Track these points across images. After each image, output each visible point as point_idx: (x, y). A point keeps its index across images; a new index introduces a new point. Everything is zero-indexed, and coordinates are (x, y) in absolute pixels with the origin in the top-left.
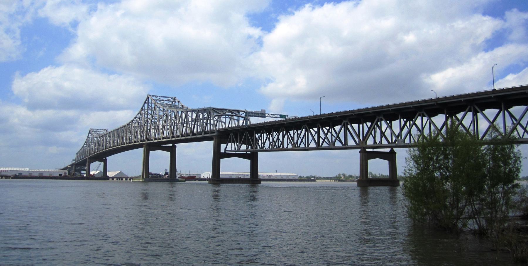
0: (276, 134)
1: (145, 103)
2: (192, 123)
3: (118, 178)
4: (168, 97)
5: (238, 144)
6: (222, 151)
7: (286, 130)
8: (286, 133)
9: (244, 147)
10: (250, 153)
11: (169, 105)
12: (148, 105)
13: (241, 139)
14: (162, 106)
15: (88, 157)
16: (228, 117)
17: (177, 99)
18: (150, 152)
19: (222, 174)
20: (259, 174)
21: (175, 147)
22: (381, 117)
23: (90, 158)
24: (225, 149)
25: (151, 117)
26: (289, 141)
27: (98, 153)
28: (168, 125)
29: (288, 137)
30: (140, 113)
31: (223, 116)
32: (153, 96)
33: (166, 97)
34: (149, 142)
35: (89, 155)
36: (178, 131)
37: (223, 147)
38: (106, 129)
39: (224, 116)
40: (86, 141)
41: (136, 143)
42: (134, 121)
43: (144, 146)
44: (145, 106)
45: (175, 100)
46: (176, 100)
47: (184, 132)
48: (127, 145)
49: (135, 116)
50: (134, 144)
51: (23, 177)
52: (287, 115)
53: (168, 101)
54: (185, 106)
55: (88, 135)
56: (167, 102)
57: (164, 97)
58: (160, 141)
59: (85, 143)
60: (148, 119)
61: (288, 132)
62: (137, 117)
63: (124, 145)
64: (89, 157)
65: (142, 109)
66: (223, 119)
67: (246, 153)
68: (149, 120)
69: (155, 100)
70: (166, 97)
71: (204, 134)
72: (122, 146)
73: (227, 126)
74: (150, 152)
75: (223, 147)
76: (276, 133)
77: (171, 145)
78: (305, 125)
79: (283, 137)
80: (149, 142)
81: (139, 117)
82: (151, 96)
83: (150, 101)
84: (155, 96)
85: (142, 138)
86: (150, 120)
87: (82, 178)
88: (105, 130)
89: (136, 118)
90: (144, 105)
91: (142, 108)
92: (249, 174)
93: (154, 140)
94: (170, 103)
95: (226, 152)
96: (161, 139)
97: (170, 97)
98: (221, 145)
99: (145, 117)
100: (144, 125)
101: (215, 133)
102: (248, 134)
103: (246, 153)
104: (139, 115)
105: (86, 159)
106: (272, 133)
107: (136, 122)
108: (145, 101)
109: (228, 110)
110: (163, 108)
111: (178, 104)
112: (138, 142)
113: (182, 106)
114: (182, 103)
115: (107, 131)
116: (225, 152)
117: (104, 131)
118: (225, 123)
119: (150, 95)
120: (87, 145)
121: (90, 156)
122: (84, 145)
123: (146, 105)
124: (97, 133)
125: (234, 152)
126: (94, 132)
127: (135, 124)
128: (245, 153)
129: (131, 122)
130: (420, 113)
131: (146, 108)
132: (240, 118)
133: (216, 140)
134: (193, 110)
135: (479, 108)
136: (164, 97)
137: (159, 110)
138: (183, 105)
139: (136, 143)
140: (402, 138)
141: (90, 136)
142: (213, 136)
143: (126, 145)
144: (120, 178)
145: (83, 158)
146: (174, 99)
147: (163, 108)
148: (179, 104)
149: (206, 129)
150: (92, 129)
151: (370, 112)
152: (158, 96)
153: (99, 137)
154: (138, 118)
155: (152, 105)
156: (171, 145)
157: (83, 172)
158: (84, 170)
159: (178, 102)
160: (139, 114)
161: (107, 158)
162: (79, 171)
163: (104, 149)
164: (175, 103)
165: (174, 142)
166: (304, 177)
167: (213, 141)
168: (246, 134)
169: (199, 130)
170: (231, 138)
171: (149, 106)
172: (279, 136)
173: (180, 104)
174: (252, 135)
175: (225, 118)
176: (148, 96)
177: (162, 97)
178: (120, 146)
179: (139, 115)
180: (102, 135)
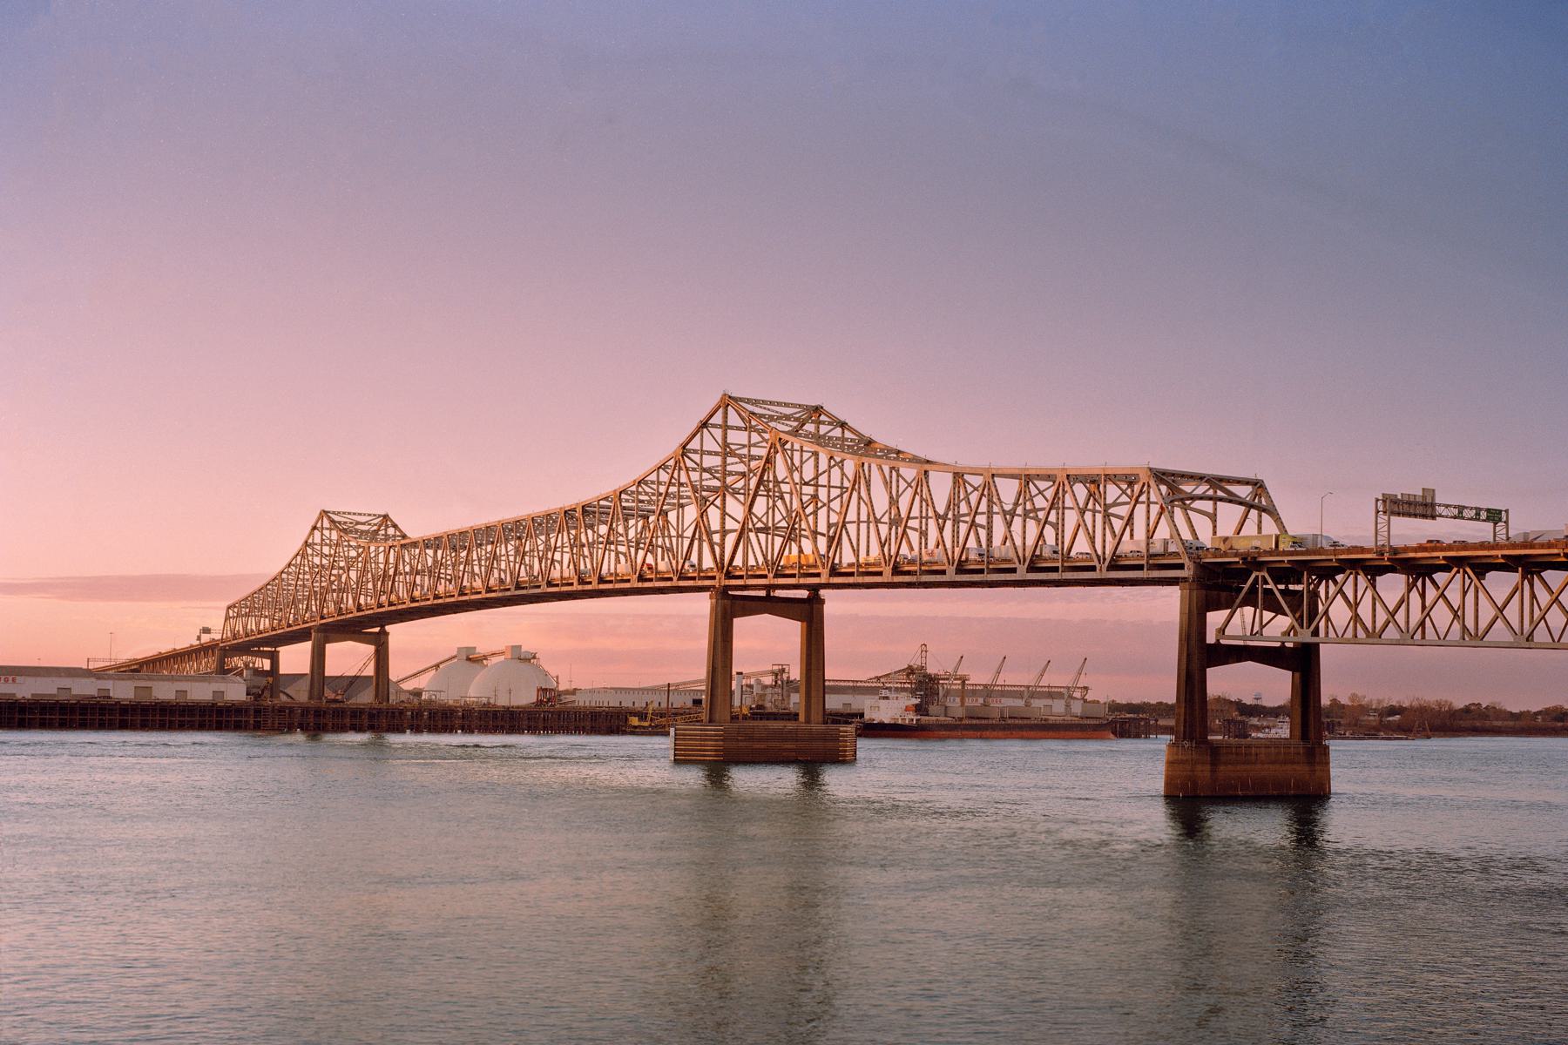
1: (314, 528)
2: (515, 559)
16: (1230, 488)
18: (737, 622)
21: (387, 634)
22: (1263, 574)
24: (1222, 631)
29: (1461, 606)
30: (302, 554)
36: (773, 554)
37: (1215, 618)
38: (383, 513)
42: (268, 587)
52: (1507, 511)
62: (294, 562)
74: (737, 622)
81: (298, 563)
89: (289, 565)
91: (306, 542)
95: (1222, 642)
99: (313, 562)
104: (299, 558)
127: (288, 575)
130: (1257, 573)
131: (317, 539)
132: (1218, 503)
133: (1195, 593)
140: (1377, 631)
161: (388, 628)
166: (785, 676)
169: (752, 562)
179: (299, 558)
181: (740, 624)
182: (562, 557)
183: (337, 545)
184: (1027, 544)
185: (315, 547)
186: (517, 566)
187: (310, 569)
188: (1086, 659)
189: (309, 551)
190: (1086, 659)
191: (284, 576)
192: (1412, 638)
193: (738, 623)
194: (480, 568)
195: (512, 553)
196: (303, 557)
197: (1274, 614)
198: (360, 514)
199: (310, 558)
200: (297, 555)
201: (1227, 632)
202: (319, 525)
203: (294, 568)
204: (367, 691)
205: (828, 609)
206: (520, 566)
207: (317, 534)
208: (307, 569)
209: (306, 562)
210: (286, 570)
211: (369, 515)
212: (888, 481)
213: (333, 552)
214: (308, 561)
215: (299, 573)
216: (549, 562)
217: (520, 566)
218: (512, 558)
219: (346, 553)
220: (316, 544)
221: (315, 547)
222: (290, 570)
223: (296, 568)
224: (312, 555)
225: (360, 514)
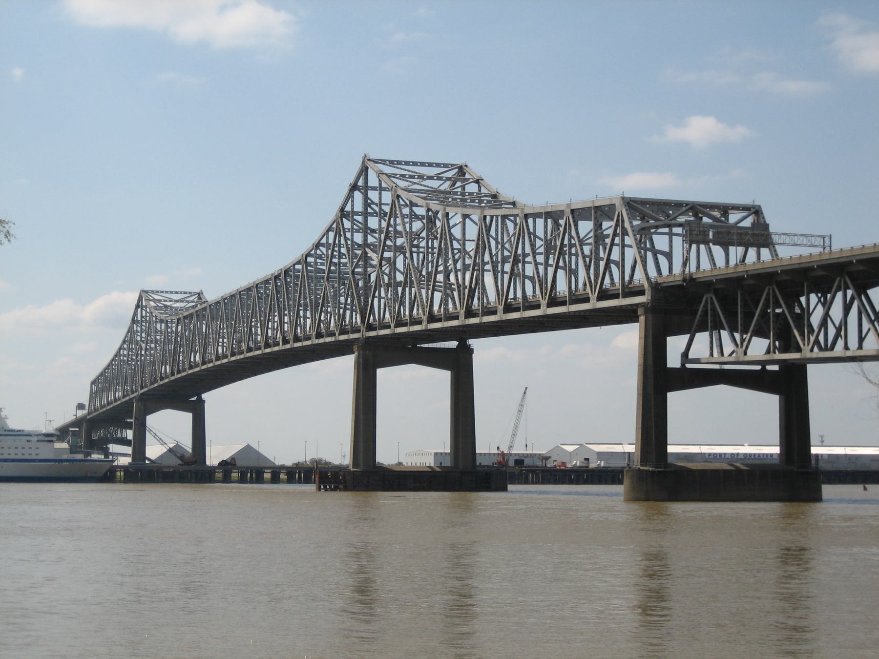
0: (819, 301)
1: (354, 187)
2: (547, 259)
3: (247, 468)
4: (438, 165)
5: (737, 336)
6: (673, 361)
7: (854, 286)
8: (856, 296)
9: (758, 347)
10: (776, 368)
11: (443, 192)
12: (366, 198)
13: (749, 316)
14: (422, 198)
15: (135, 394)
17: (475, 169)
18: (381, 372)
19: (480, 454)
20: (477, 452)
21: (470, 351)
23: (143, 398)
24: (685, 355)
25: (380, 241)
26: (866, 325)
27: (173, 378)
28: (441, 272)
30: (336, 228)
31: (660, 230)
32: (384, 162)
33: (430, 165)
34: (373, 334)
35: (142, 388)
37: (675, 345)
39: (666, 230)
40: (126, 336)
41: (321, 341)
42: (310, 259)
43: (355, 348)
44: (353, 201)
45: (465, 174)
46: (467, 176)
47: (436, 308)
48: (288, 346)
49: (314, 239)
50: (317, 341)
51: (533, 470)
53: (440, 179)
54: (506, 194)
55: (135, 314)
56: (435, 184)
57: (422, 164)
58: (417, 328)
59: (124, 342)
60: (368, 250)
61: (862, 289)
63: (276, 349)
64: (142, 394)
65: (343, 213)
66: (661, 242)
67: (764, 368)
68: (370, 254)
69: (389, 176)
70: (430, 165)
71: (599, 299)
72: (268, 350)
73: (677, 269)
74: (381, 372)
75: (675, 345)
76: (820, 295)
77: (453, 344)
78: (708, 293)
79: (847, 309)
80: (373, 334)
81: (331, 241)
82: (376, 162)
83: (373, 181)
84: (392, 163)
85: (299, 331)
86: (375, 252)
87: (108, 476)
88: (195, 294)
89: (318, 245)
90: (350, 196)
91: (342, 210)
92: (776, 450)
93: (337, 333)
94: (446, 186)
95: (688, 366)
96: (424, 323)
97: (445, 165)
98: (670, 339)
99: (352, 241)
100: (353, 272)
101: (642, 293)
102: (716, 302)
103: (764, 368)
105: (130, 402)
106: (829, 296)
107: (318, 261)
108: (352, 180)
109: (687, 205)
110: (427, 205)
111: (477, 191)
112: (332, 334)
113: (495, 196)
114: (494, 183)
115: (200, 298)
116: (683, 365)
117: (191, 299)
118: (669, 256)
119: (371, 158)
120: (130, 349)
121: (146, 389)
122: (120, 349)
123: (358, 196)
124: (166, 306)
125: (717, 367)
126: (155, 300)
127: (316, 258)
128: (758, 368)
129: (298, 263)
130: (769, 287)
131: (359, 206)
133: (650, 319)
134: (549, 210)
135: (852, 281)
136: (422, 164)
137: (411, 215)
138: (494, 192)
139: (321, 341)
141: (142, 317)
142: (637, 305)
143: (281, 347)
144: (254, 468)
145: (109, 403)
146: (461, 170)
147: (427, 205)
148: (479, 187)
149: (511, 295)
150: (146, 292)
151: (712, 280)
152: (399, 163)
153: (176, 321)
154: (328, 246)
155: (380, 198)
156: (453, 344)
157: (114, 448)
158: (124, 442)
159: (477, 181)
160: (329, 229)
161: (204, 396)
162: (101, 446)
163: (197, 366)
164: (463, 187)
165: (464, 334)
167: (636, 326)
168: (768, 294)
170: (705, 312)
171: (369, 201)
172: (829, 309)
173: (483, 190)
174: (792, 298)
175: (671, 235)
176: (363, 162)
177: (415, 164)
178: (258, 352)
179: (331, 235)
180: (186, 314)
181: (385, 376)
182: (623, 253)
183: (393, 214)
184: (635, 278)
185: (355, 217)
186: (551, 271)
187: (348, 249)
188: (526, 388)
189: (347, 224)
190: (526, 388)
191: (310, 259)
192: (745, 354)
193: (382, 373)
194: (546, 269)
195: (542, 250)
196: (338, 234)
197: (686, 337)
198: (171, 292)
199: (348, 235)
200: (328, 231)
201: (691, 356)
202: (360, 183)
203: (324, 250)
204: (181, 461)
205: (477, 359)
206: (555, 272)
207: (358, 196)
208: (343, 250)
209: (343, 241)
210: (313, 252)
211: (185, 293)
212: (567, 235)
213: (384, 224)
214: (346, 239)
215: (333, 256)
216: (602, 264)
217: (555, 272)
218: (540, 259)
219: (407, 226)
220: (357, 214)
221: (355, 217)
222: (318, 252)
223: (328, 249)
224: (352, 230)
225: (171, 292)
